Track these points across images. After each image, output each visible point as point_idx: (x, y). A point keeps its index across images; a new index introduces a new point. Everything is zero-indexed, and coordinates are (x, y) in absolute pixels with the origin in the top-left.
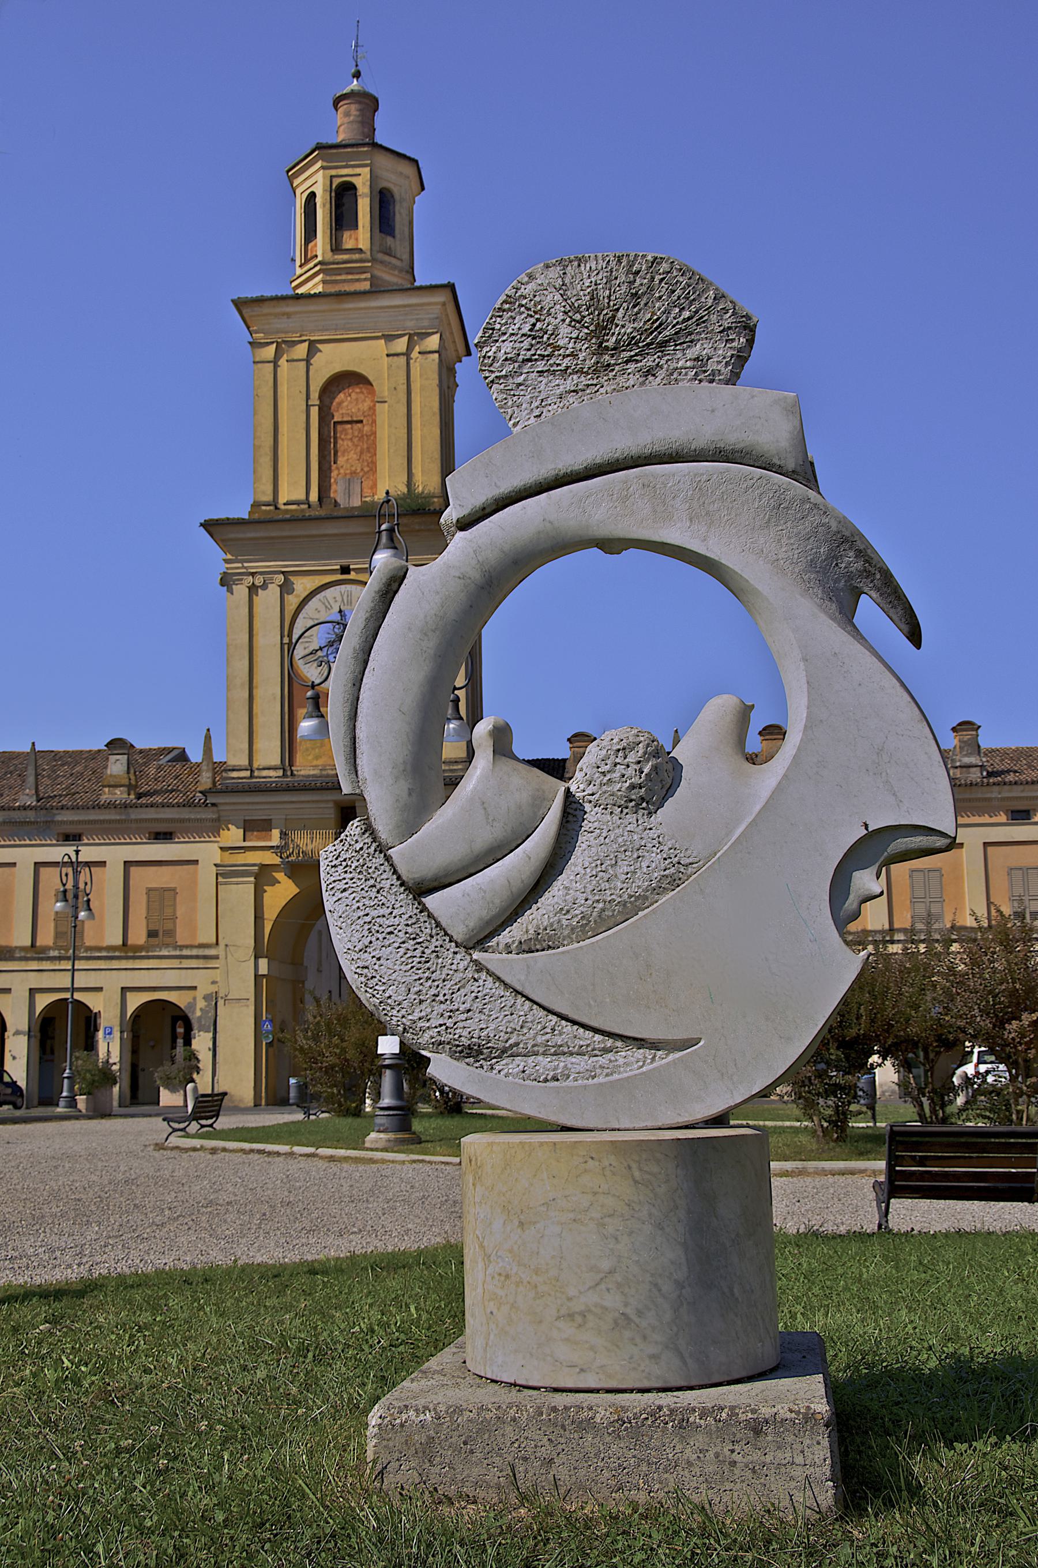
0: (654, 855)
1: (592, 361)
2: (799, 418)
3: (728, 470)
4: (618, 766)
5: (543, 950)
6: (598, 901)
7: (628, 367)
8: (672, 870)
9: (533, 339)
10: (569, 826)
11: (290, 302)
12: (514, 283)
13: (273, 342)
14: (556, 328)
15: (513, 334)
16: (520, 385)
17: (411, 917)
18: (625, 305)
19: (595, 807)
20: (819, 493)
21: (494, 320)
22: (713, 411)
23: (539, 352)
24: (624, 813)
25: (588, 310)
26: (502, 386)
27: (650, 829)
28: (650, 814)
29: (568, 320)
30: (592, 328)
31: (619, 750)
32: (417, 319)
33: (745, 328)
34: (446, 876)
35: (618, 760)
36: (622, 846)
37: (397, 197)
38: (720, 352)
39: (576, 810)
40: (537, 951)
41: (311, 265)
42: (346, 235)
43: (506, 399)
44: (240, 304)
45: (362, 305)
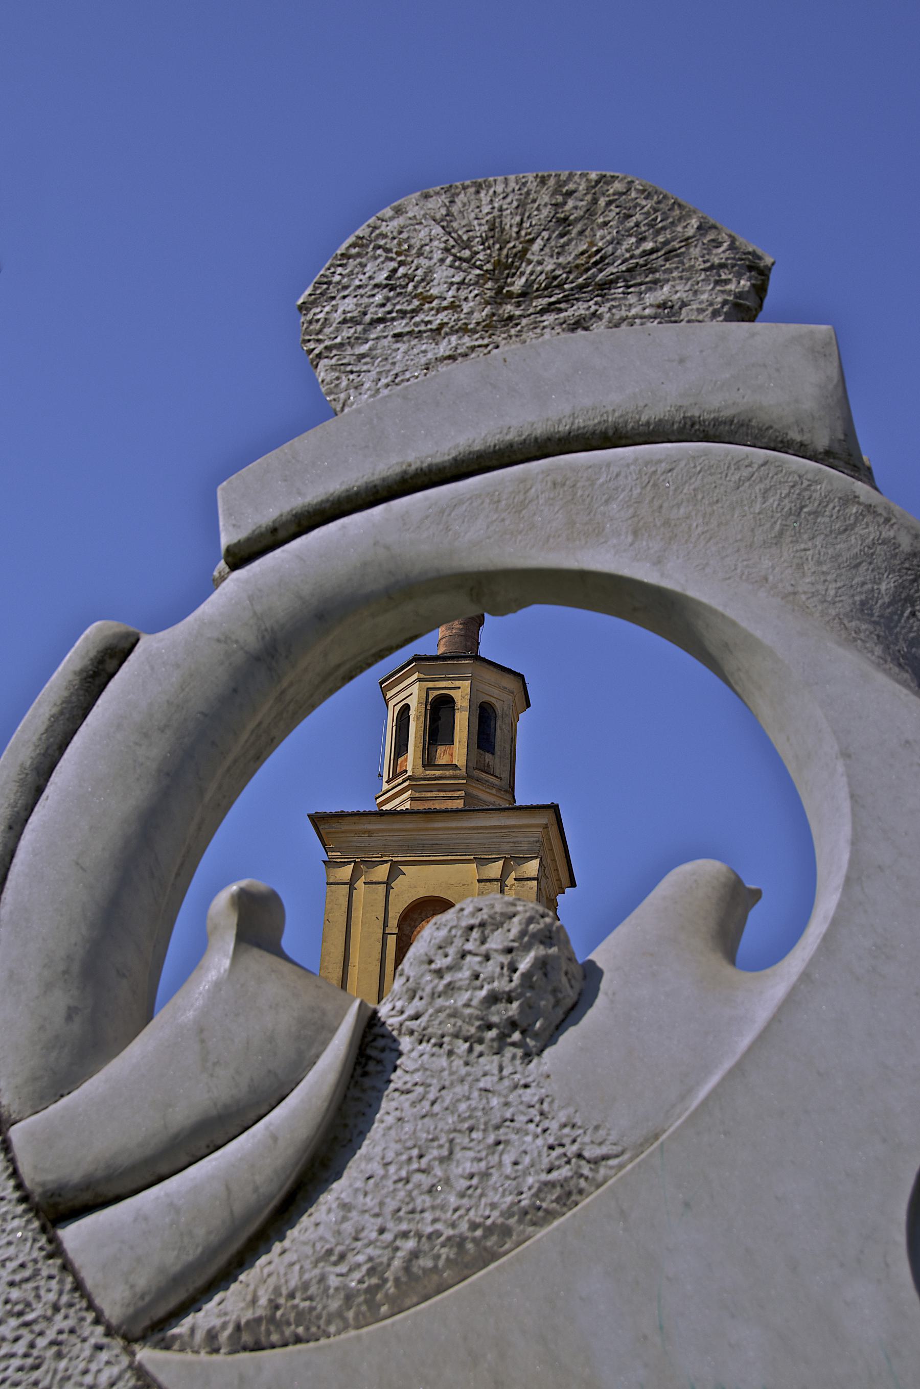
0: (529, 1139)
1: (484, 314)
2: (836, 364)
3: (706, 453)
4: (469, 958)
5: (285, 1345)
6: (405, 1235)
7: (545, 318)
8: (565, 1172)
9: (391, 290)
10: (367, 1082)
11: (373, 818)
12: (371, 221)
13: (351, 862)
14: (430, 271)
15: (359, 287)
16: (363, 356)
17: (22, 1266)
18: (545, 234)
19: (421, 1042)
20: (876, 489)
21: (332, 270)
22: (682, 361)
23: (398, 307)
24: (476, 1053)
25: (483, 244)
26: (333, 361)
27: (526, 1086)
28: (528, 1056)
29: (450, 258)
30: (488, 267)
31: (471, 928)
32: (514, 842)
33: (751, 268)
34: (108, 1179)
35: (469, 946)
36: (463, 1120)
37: (499, 712)
38: (705, 297)
39: (383, 1050)
40: (273, 1347)
41: (400, 780)
42: (441, 749)
43: (338, 378)
44: (317, 820)
45: (454, 824)
